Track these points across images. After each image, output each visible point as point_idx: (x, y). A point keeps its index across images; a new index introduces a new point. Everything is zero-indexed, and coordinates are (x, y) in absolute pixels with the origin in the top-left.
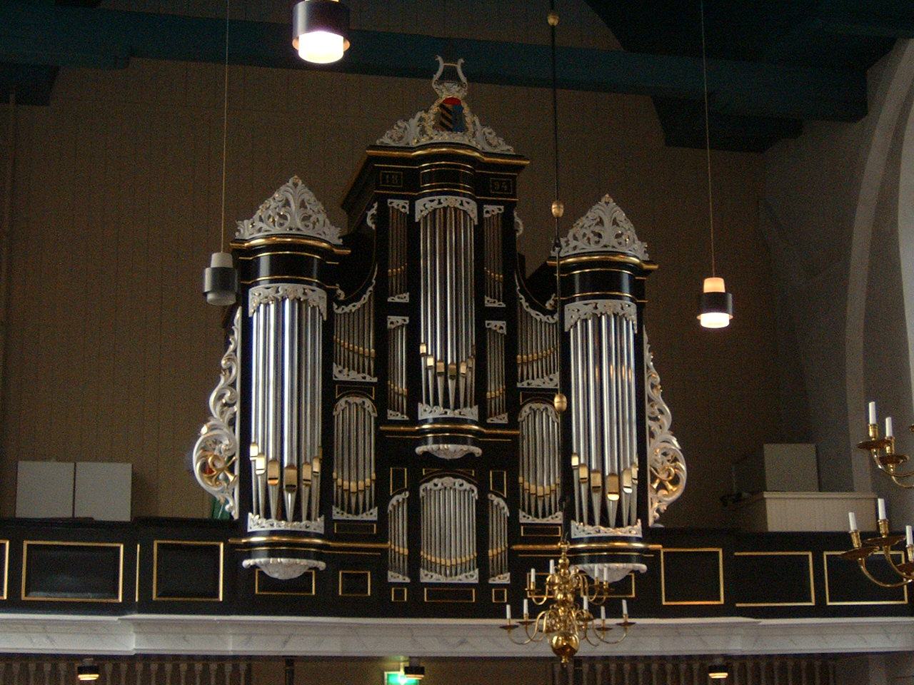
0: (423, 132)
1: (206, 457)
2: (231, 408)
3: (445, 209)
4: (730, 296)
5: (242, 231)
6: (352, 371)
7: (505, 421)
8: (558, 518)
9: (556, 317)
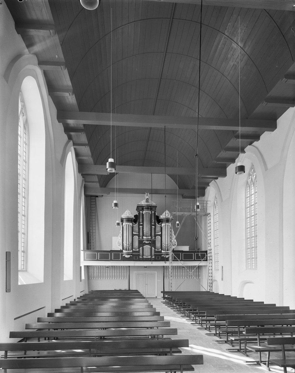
8: (160, 250)
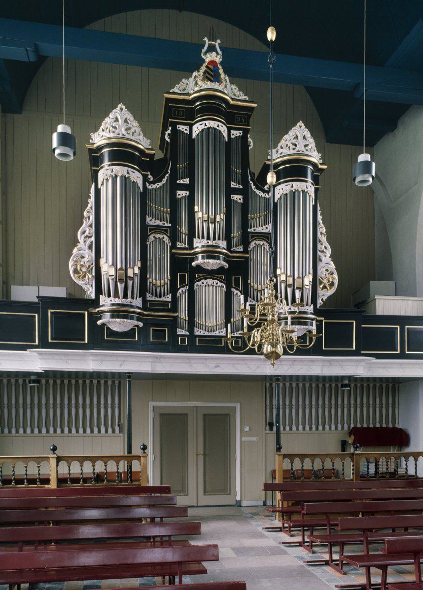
0: (196, 84)
1: (76, 265)
2: (90, 239)
3: (208, 129)
4: (374, 164)
5: (93, 139)
6: (157, 220)
7: (241, 250)
9: (270, 194)
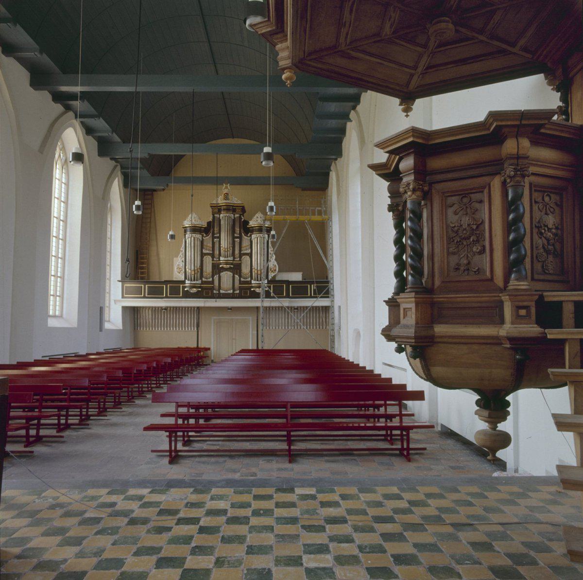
8: (249, 279)
